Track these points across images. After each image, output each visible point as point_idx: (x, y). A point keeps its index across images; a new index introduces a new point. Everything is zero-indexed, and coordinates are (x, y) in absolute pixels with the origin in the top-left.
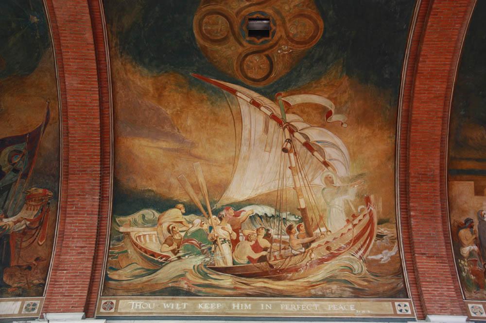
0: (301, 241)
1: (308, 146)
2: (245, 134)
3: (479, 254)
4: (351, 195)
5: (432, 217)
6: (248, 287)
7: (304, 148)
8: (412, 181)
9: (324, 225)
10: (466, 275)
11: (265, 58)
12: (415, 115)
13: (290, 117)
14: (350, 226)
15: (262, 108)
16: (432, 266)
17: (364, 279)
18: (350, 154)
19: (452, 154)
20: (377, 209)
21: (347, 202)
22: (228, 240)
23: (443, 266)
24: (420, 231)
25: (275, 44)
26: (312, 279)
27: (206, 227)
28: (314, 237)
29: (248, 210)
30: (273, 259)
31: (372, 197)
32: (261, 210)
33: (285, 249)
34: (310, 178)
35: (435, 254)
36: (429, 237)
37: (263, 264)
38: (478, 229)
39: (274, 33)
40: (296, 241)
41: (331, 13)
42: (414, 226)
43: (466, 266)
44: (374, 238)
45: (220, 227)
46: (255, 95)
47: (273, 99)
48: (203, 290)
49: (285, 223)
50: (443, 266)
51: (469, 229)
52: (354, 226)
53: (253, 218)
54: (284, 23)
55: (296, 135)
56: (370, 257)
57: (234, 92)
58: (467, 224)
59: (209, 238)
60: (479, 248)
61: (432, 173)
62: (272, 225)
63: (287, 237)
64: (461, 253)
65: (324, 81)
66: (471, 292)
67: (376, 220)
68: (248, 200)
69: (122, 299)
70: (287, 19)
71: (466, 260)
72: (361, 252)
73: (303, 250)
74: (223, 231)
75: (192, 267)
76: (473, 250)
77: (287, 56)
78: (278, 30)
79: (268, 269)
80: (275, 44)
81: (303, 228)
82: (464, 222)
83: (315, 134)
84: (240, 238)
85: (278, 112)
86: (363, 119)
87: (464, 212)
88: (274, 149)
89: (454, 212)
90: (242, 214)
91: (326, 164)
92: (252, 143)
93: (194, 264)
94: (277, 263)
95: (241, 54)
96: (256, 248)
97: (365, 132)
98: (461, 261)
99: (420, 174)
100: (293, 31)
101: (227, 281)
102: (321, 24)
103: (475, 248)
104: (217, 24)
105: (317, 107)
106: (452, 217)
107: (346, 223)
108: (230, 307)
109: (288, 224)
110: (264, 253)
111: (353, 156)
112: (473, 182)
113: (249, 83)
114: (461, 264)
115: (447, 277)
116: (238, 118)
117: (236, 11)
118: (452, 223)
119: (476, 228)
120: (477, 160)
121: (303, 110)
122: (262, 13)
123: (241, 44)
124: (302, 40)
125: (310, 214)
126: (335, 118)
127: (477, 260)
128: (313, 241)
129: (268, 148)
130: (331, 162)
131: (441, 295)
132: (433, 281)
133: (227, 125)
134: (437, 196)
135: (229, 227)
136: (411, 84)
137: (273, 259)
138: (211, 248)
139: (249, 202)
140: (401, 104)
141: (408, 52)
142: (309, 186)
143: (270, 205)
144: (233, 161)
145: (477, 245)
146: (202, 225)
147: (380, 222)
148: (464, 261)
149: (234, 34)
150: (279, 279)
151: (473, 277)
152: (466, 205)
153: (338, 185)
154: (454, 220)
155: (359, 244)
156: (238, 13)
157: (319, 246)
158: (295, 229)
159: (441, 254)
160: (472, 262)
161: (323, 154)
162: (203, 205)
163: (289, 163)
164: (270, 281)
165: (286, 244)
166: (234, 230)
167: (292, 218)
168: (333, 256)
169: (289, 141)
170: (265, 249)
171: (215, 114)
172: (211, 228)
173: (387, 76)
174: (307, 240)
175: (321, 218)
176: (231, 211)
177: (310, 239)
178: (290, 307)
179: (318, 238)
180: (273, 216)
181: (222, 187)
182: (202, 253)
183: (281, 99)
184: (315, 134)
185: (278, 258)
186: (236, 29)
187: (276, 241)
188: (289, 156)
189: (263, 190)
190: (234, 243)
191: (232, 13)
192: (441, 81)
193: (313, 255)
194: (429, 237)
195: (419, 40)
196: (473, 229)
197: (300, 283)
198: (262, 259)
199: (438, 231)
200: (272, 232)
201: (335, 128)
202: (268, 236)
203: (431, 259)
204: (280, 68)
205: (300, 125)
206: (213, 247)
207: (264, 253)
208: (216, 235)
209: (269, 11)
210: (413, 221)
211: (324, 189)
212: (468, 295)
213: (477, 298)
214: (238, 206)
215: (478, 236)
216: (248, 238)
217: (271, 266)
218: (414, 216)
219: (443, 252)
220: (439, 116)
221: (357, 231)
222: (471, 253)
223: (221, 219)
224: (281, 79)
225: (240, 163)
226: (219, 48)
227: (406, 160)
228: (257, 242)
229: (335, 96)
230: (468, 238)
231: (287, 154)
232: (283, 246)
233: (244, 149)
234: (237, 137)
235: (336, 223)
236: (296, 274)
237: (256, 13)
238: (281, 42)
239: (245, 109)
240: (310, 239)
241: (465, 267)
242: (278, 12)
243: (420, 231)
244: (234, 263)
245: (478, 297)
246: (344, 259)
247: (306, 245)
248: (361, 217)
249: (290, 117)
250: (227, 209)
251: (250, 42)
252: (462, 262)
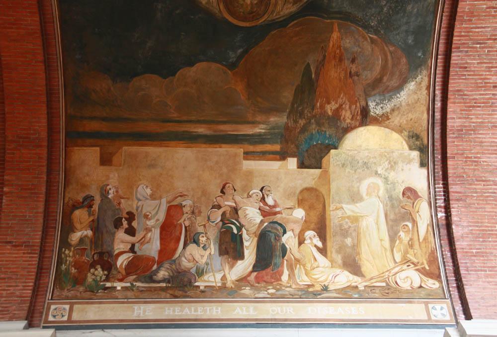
3: (91, 241)
5: (32, 193)
10: (66, 269)
16: (16, 257)
23: (30, 257)
24: (13, 212)
35: (25, 242)
36: (22, 220)
38: (99, 209)
42: (6, 207)
43: (69, 256)
50: (30, 257)
51: (86, 209)
58: (86, 203)
60: (94, 234)
61: (37, 136)
64: (69, 240)
66: (64, 289)
69: (76, 303)
71: (72, 249)
76: (86, 236)
82: (81, 200)
87: (84, 186)
89: (71, 187)
98: (65, 251)
99: (21, 138)
103: (89, 233)
106: (67, 194)
112: (98, 149)
114: (64, 253)
115: (29, 272)
118: (66, 202)
119: (96, 207)
120: (104, 119)
124: (353, 27)
127: (86, 249)
132: (8, 278)
134: (43, 166)
145: (92, 230)
148: (70, 250)
151: (73, 270)
152: (87, 178)
154: (69, 198)
159: (32, 242)
160: (79, 251)
178: (174, 311)
192: (30, 12)
194: (22, 220)
196: (92, 209)
199: (37, 213)
203: (18, 248)
212: (58, 293)
213: (68, 297)
215: (96, 217)
218: (7, 193)
219: (36, 239)
220: (39, 60)
222: (82, 240)
230: (82, 221)
241: (68, 258)
243: (13, 212)
245: (70, 295)
252: (67, 252)
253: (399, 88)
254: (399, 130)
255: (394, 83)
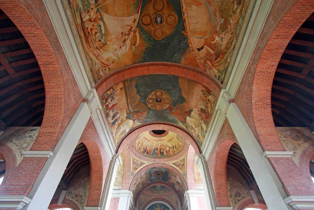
0: (98, 45)
1: (125, 40)
2: (125, 18)
4: (114, 57)
6: (80, 30)
7: (124, 40)
8: (122, 73)
9: (104, 52)
11: (149, 23)
12: (138, 69)
13: (132, 33)
14: (106, 60)
15: (134, 23)
17: (95, 70)
18: (124, 54)
19: (128, 80)
20: (112, 66)
21: (112, 57)
22: (90, 17)
25: (154, 26)
26: (90, 54)
27: (92, 6)
28: (100, 50)
29: (102, 24)
30: (90, 37)
31: (114, 64)
32: (103, 28)
33: (94, 41)
34: (116, 43)
37: (88, 34)
39: (157, 25)
40: (97, 44)
41: (163, 41)
44: (104, 68)
45: (94, 13)
46: (137, 21)
47: (137, 27)
48: (73, 10)
49: (101, 38)
52: (106, 61)
53: (100, 26)
54: (160, 28)
55: (127, 36)
56: (100, 69)
57: (138, 13)
59: (89, 9)
62: (100, 34)
63: (97, 40)
65: (144, 42)
67: (109, 67)
68: (105, 23)
70: (161, 29)
72: (101, 66)
73: (96, 47)
74: (93, 15)
75: (78, 3)
77: (150, 30)
78: (158, 26)
79: (87, 37)
80: (154, 26)
81: (101, 45)
83: (128, 42)
84: (92, 22)
85: (133, 29)
86: (134, 55)
87: (116, 88)
88: (122, 29)
90: (100, 21)
91: (120, 47)
92: (123, 21)
93: (79, 4)
94: (89, 40)
95: (150, 14)
96: (91, 30)
97: (131, 57)
100: (158, 31)
101: (79, 21)
102: (160, 39)
104: (160, 6)
105: (136, 41)
107: (106, 58)
108: (72, 25)
109: (101, 40)
110: (91, 33)
111: (124, 55)
113: (141, 18)
116: (130, 15)
117: (164, 12)
121: (135, 37)
122: (163, 21)
123: (153, 14)
125: (106, 46)
126: (134, 47)
128: (99, 50)
129: (122, 27)
130: (121, 49)
131: (100, 92)
133: (127, 11)
135: (94, 17)
136: (145, 65)
137: (90, 37)
138: (86, 10)
139: (104, 23)
140: (139, 64)
141: (153, 62)
142: (113, 44)
143: (105, 31)
144: (115, 15)
146: (92, 4)
147: (109, 68)
149: (157, 12)
150: (86, 42)
153: (116, 53)
155: (102, 65)
156: (163, 13)
157: (98, 52)
158: (101, 42)
161: (123, 46)
162: (99, 4)
163: (119, 35)
164: (84, 39)
165: (95, 41)
166: (94, 19)
167: (103, 41)
168: (97, 58)
169: (125, 34)
170: (92, 34)
171: (130, 6)
172: (92, 9)
173: (146, 59)
174: (99, 48)
175: (106, 50)
176: (100, 17)
177: (99, 49)
179: (100, 51)
180: (102, 33)
181: (107, 12)
182: (84, 7)
183: (137, 29)
184: (128, 42)
185: (91, 39)
186: (158, 13)
187: (95, 36)
188: (120, 35)
189: (109, 29)
190: (90, 20)
191: (164, 11)
193: (95, 51)
195: (157, 65)
197: (87, 49)
198: (89, 33)
200: (98, 34)
201: (131, 48)
202: (96, 33)
204: (146, 28)
205: (130, 37)
206: (87, 11)
207: (91, 33)
208: (91, 12)
209: (164, 23)
210: (112, 77)
211: (113, 48)
214: (102, 19)
216: (93, 25)
217: (88, 37)
221: (105, 62)
223: (96, 13)
224: (143, 29)
225: (116, 18)
226: (152, 6)
227: (125, 70)
228: (93, 29)
229: (140, 46)
231: (121, 34)
232: (95, 40)
233: (120, 18)
234: (123, 16)
235: (106, 55)
236: (89, 48)
237: (164, 19)
238: (154, 27)
239: (133, 17)
240: (99, 49)
242: (164, 26)
244: (85, 22)
246: (97, 62)
247: (97, 48)
248: (109, 62)
249: (132, 33)
250: (100, 15)
251: (154, 18)
253: (139, 122)
254: (133, 125)
255: (139, 121)
